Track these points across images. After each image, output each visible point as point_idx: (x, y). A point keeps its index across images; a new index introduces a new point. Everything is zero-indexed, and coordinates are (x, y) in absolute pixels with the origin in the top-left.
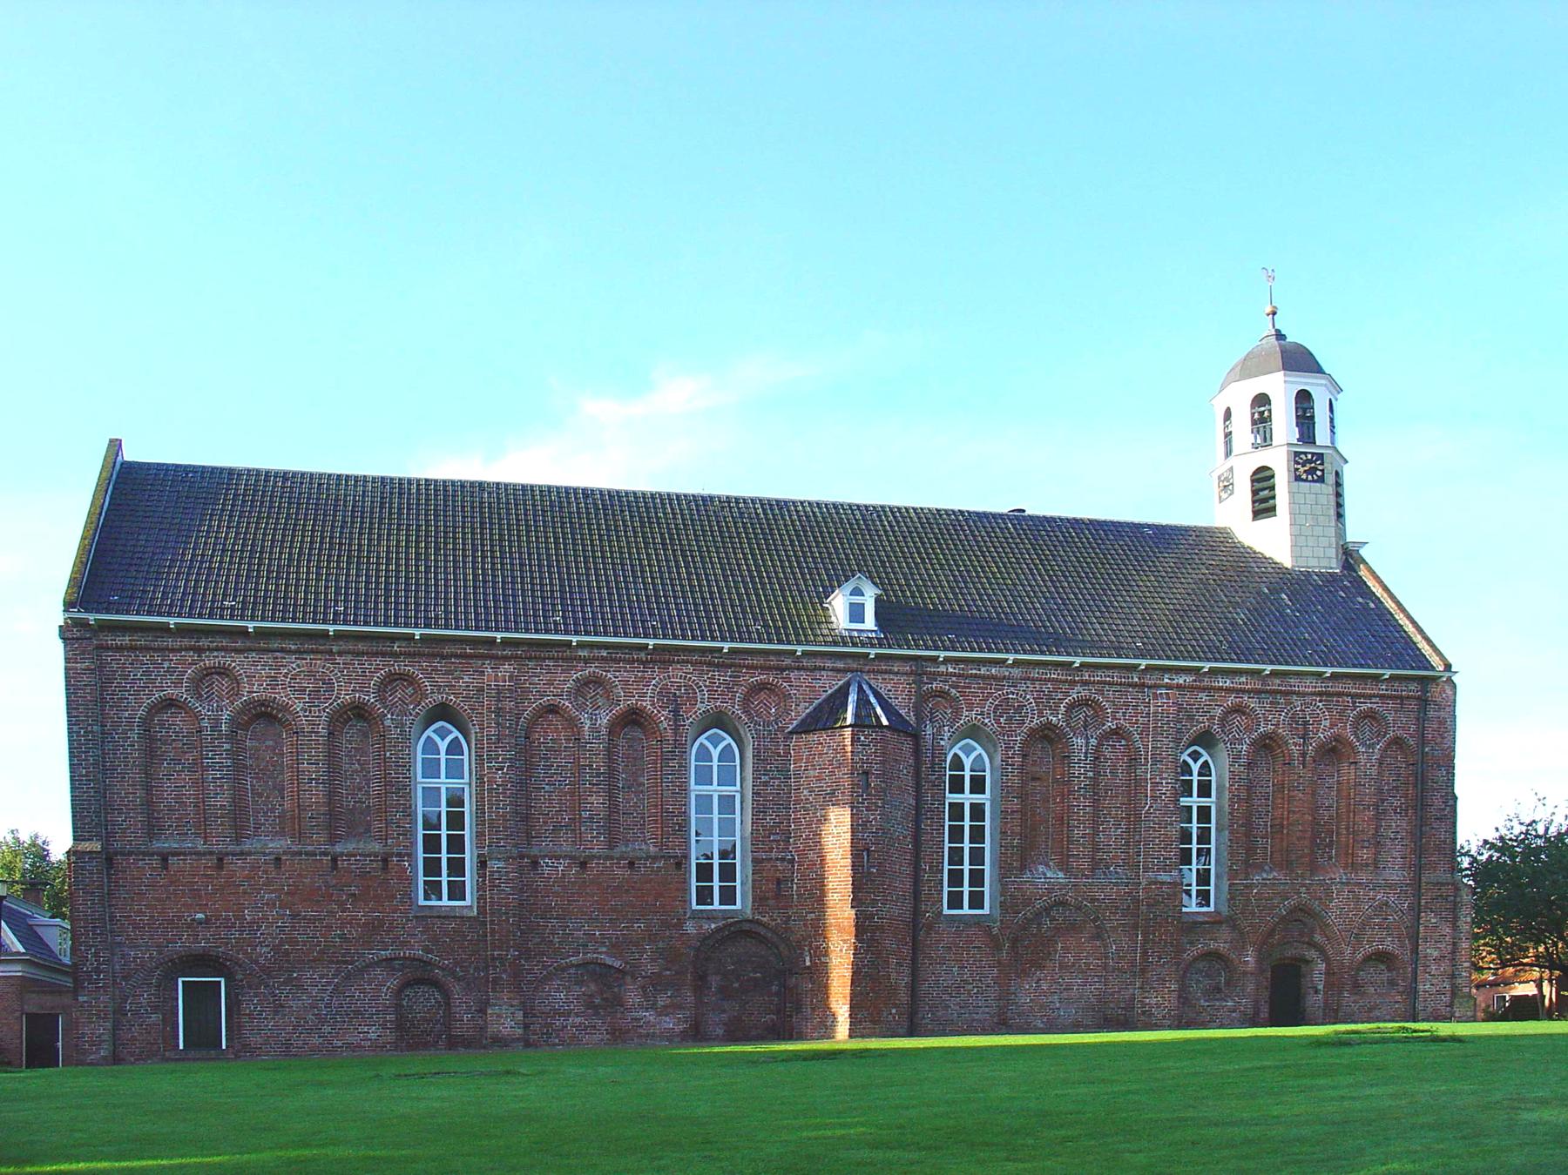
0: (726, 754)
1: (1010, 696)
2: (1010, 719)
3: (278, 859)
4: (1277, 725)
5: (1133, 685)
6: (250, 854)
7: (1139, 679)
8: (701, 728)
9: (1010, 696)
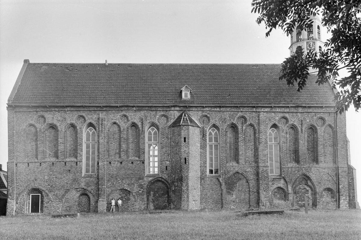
0: (155, 133)
1: (223, 116)
2: (222, 122)
3: (53, 163)
4: (294, 122)
5: (254, 112)
6: (47, 162)
7: (256, 110)
8: (149, 126)
9: (223, 116)
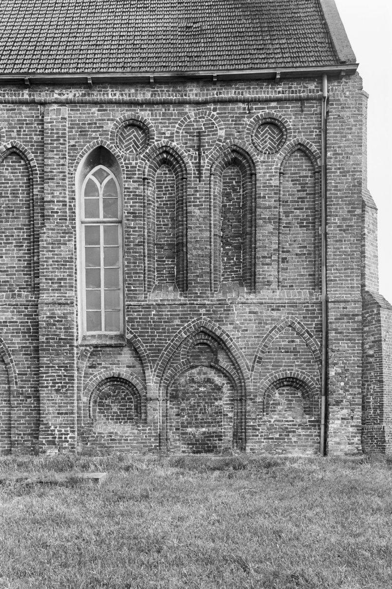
7: (30, 95)
